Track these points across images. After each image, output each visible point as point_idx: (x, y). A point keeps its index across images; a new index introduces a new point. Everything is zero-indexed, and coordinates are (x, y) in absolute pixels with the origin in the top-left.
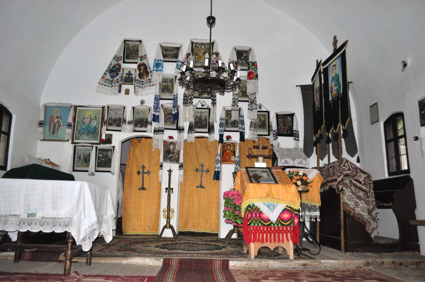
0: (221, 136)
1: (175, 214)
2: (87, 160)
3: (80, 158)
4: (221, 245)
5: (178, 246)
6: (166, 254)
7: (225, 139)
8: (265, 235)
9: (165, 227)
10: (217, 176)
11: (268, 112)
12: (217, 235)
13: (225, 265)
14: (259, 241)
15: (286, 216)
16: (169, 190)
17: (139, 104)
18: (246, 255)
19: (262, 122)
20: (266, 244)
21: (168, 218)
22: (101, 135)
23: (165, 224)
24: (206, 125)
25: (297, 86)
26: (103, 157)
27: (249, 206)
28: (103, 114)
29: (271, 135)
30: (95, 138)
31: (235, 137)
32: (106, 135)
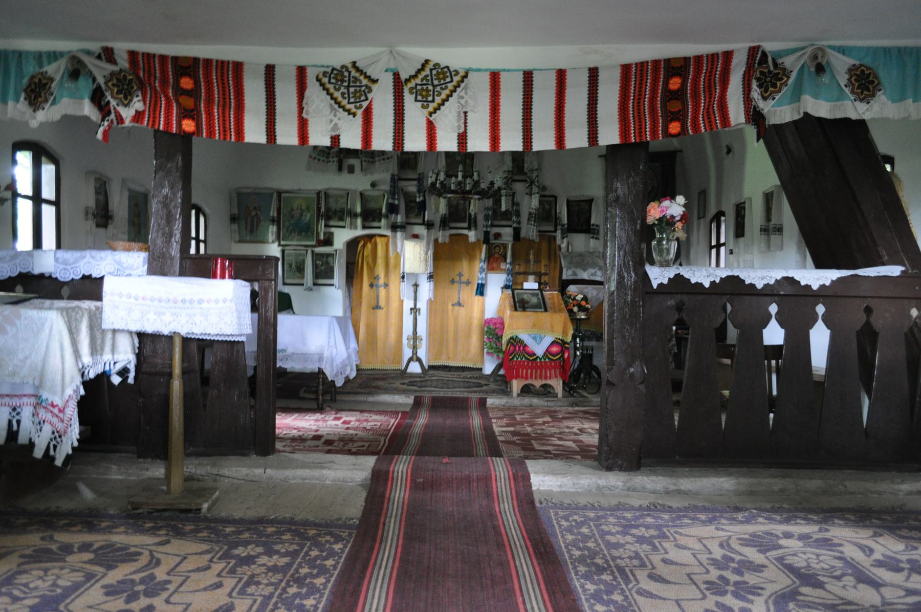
0: (487, 234)
1: (424, 342)
2: (300, 269)
3: (290, 266)
4: (483, 383)
5: (428, 383)
6: (416, 391)
7: (491, 237)
8: (529, 371)
9: (410, 360)
10: (481, 290)
11: (555, 197)
12: (481, 369)
13: (482, 403)
14: (522, 377)
15: (555, 349)
16: (415, 310)
17: (369, 187)
18: (506, 392)
19: (546, 214)
20: (529, 382)
21: (415, 348)
22: (318, 234)
23: (411, 355)
24: (465, 217)
25: (600, 156)
26: (322, 265)
27: (512, 338)
28: (319, 203)
29: (559, 232)
30: (308, 238)
31: (507, 234)
32: (325, 234)
